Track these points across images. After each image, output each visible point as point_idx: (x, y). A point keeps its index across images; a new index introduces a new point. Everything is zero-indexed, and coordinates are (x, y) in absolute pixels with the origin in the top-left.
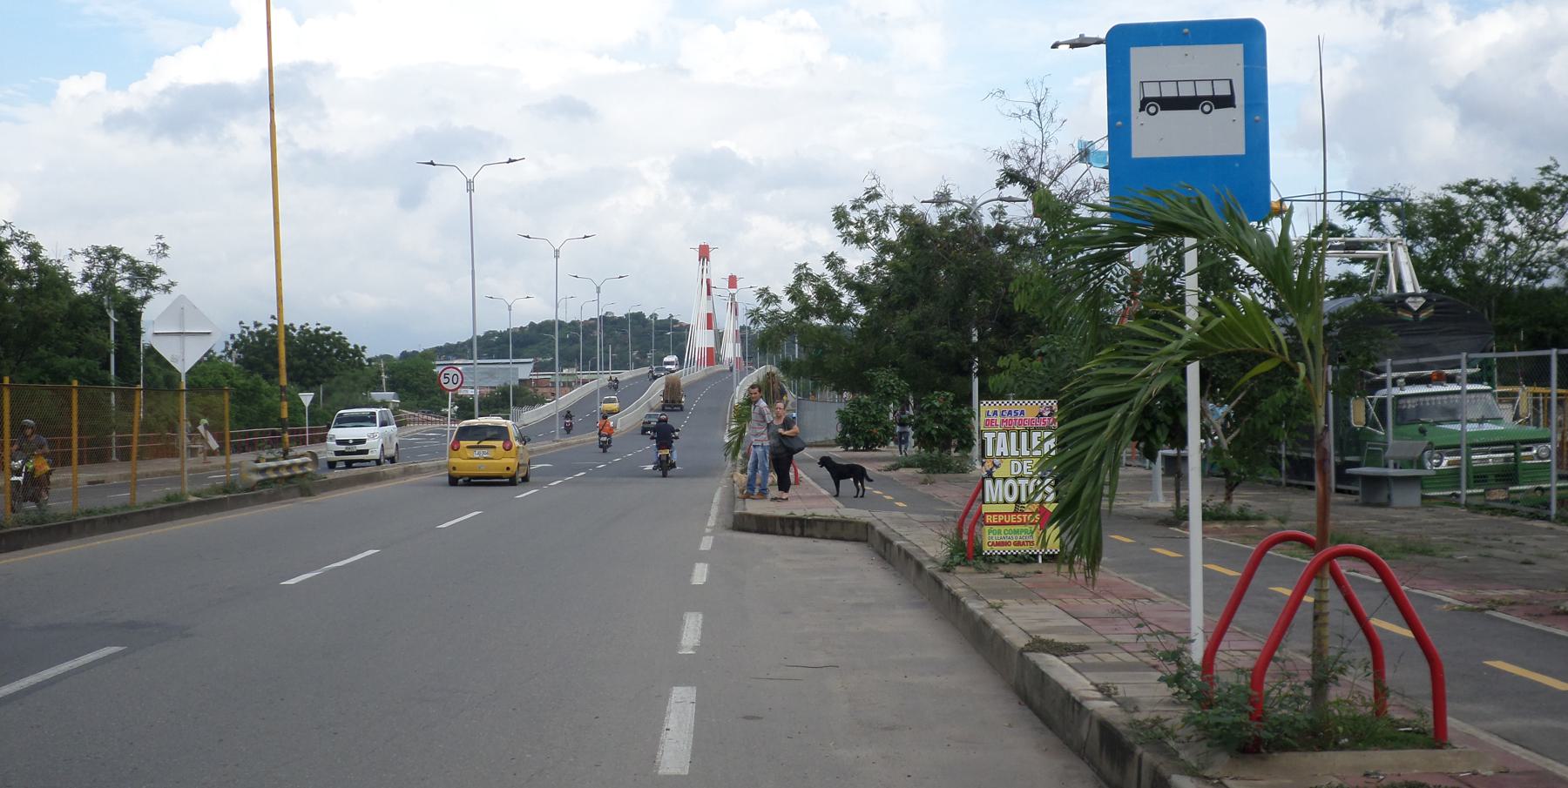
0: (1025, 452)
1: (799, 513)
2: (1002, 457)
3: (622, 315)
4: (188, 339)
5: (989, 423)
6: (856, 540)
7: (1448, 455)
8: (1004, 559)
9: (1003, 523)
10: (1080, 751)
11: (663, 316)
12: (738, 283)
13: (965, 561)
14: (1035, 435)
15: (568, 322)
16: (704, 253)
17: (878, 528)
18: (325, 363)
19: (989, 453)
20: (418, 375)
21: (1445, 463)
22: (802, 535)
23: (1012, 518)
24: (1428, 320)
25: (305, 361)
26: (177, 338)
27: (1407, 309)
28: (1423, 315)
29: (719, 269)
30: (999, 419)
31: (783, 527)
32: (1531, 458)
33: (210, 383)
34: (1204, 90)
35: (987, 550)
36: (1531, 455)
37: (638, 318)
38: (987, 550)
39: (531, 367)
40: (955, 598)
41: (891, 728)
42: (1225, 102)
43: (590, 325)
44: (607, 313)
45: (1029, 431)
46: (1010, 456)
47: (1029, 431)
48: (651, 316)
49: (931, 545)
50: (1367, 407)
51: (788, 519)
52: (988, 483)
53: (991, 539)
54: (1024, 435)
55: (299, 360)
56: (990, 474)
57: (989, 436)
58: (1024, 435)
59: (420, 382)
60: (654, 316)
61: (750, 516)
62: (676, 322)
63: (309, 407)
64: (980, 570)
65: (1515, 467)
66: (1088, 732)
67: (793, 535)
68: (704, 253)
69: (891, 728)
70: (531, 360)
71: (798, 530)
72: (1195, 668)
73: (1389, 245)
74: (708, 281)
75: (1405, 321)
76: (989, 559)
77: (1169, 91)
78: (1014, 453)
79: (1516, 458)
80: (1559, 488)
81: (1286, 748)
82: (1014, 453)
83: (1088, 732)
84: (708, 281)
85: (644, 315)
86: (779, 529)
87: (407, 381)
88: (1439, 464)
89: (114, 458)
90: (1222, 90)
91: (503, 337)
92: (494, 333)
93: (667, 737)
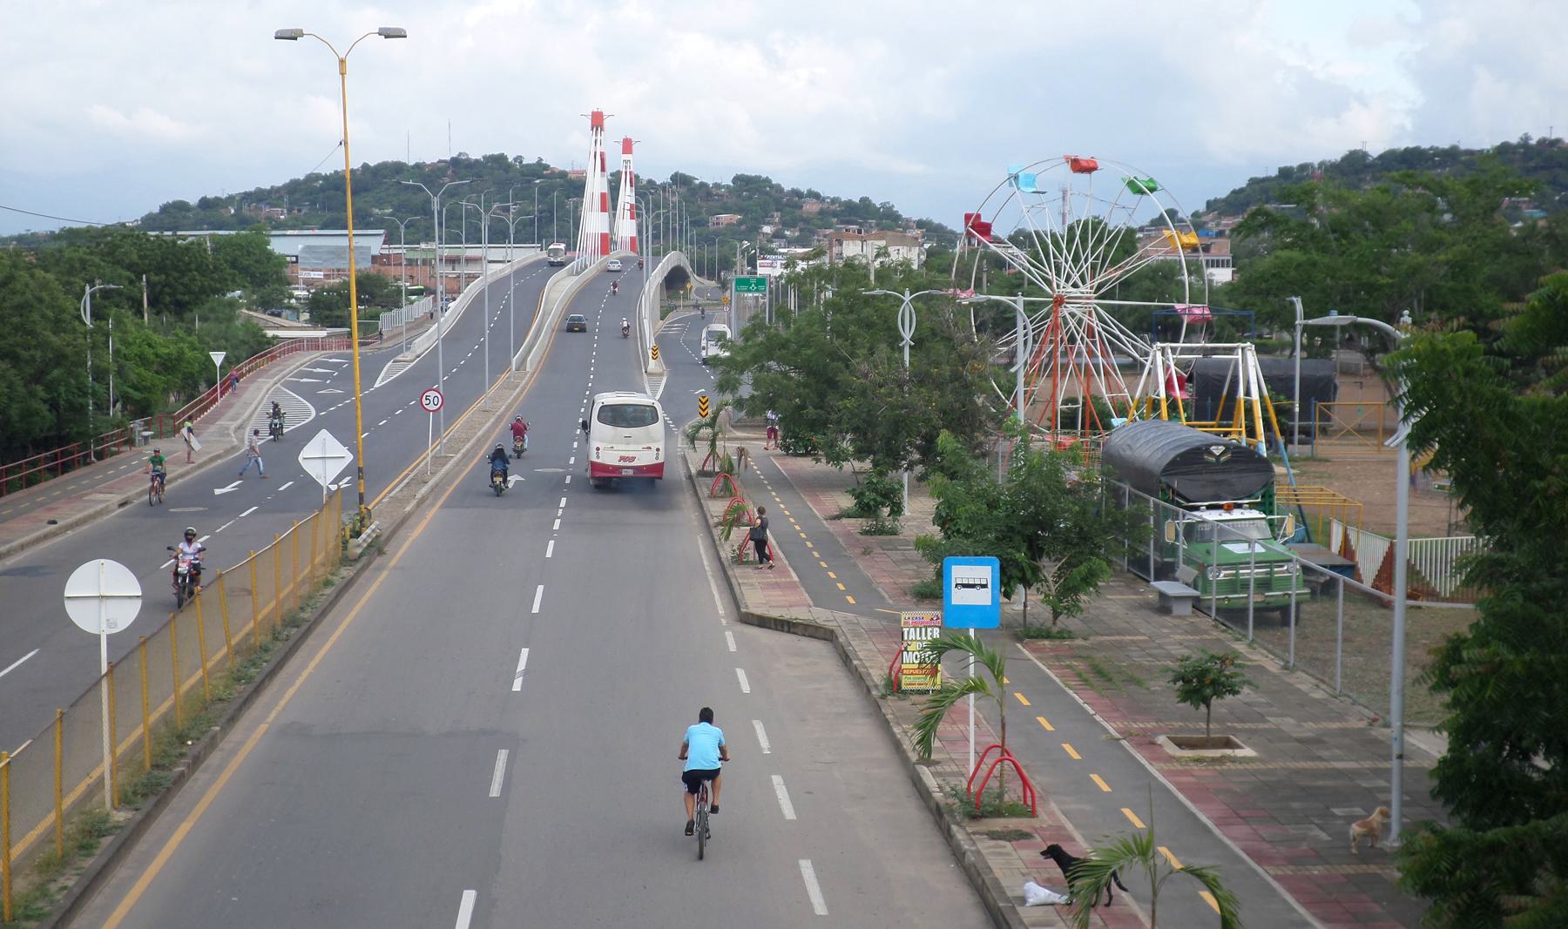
0: (924, 638)
1: (787, 617)
2: (912, 640)
3: (479, 157)
4: (327, 460)
5: (906, 623)
6: (825, 639)
7: (1225, 569)
8: (912, 692)
9: (912, 674)
10: (930, 810)
11: (530, 159)
12: (635, 147)
13: (892, 694)
14: (929, 629)
15: (412, 163)
16: (597, 121)
17: (840, 640)
18: (186, 280)
19: (906, 638)
20: (249, 253)
21: (1222, 575)
22: (789, 632)
23: (917, 671)
24: (1226, 462)
25: (163, 277)
26: (321, 461)
27: (1211, 454)
28: (1223, 459)
29: (610, 142)
30: (911, 621)
31: (776, 625)
32: (1283, 572)
33: (136, 355)
34: (977, 582)
35: (904, 687)
36: (1280, 571)
37: (499, 161)
38: (904, 687)
39: (382, 239)
40: (887, 722)
41: (863, 798)
42: (984, 586)
43: (439, 169)
44: (460, 154)
45: (926, 627)
46: (916, 640)
47: (926, 627)
48: (515, 159)
49: (877, 675)
50: (1176, 530)
51: (781, 621)
52: (905, 653)
53: (906, 682)
54: (923, 629)
55: (156, 275)
56: (906, 649)
57: (906, 630)
58: (923, 629)
59: (252, 262)
60: (519, 159)
61: (752, 615)
62: (546, 167)
63: (221, 367)
64: (900, 699)
65: (1270, 579)
66: (932, 805)
67: (783, 631)
68: (597, 121)
69: (863, 798)
70: (382, 231)
71: (786, 628)
72: (1486, 324)
73: (1240, 351)
74: (602, 155)
75: (1210, 463)
76: (905, 692)
77: (965, 582)
78: (919, 638)
79: (1270, 573)
80: (1297, 594)
81: (986, 817)
82: (919, 638)
83: (932, 805)
84: (602, 155)
85: (506, 158)
86: (773, 626)
87: (236, 259)
88: (1218, 576)
89: (93, 459)
90: (984, 582)
91: (334, 183)
92: (317, 177)
93: (781, 802)
